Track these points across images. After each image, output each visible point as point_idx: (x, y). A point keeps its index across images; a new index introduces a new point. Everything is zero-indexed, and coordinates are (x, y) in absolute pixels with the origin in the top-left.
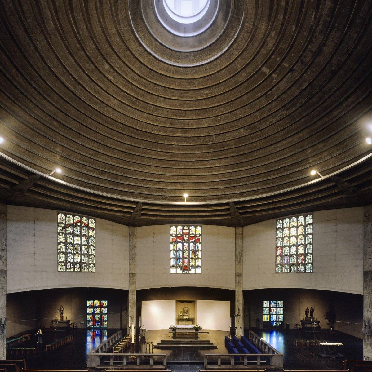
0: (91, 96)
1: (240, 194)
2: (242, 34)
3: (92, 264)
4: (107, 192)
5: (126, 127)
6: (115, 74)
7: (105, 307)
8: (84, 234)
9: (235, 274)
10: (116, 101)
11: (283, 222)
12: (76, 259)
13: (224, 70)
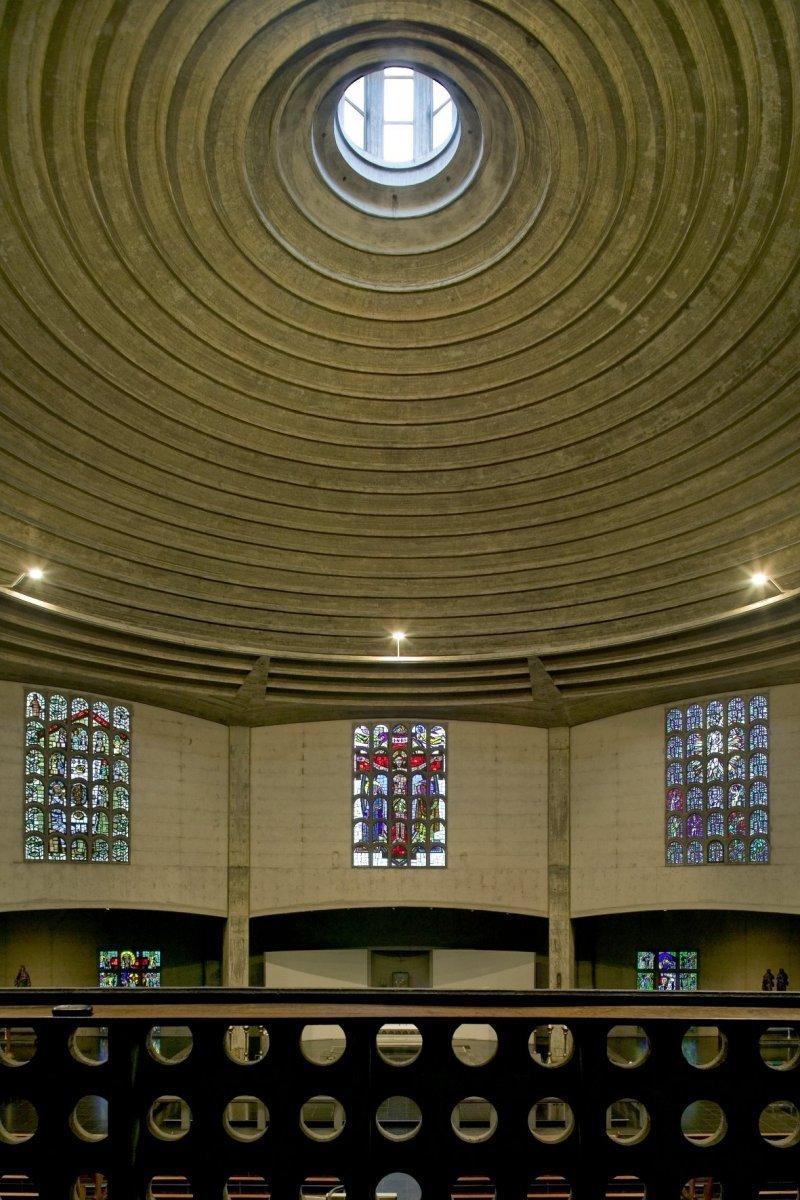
0: (133, 370)
1: (558, 631)
2: (548, 217)
3: (121, 838)
4: (168, 628)
5: (226, 446)
6: (201, 311)
7: (155, 970)
8: (98, 750)
9: (549, 866)
10: (201, 380)
11: (685, 714)
12: (74, 824)
13: (504, 301)
